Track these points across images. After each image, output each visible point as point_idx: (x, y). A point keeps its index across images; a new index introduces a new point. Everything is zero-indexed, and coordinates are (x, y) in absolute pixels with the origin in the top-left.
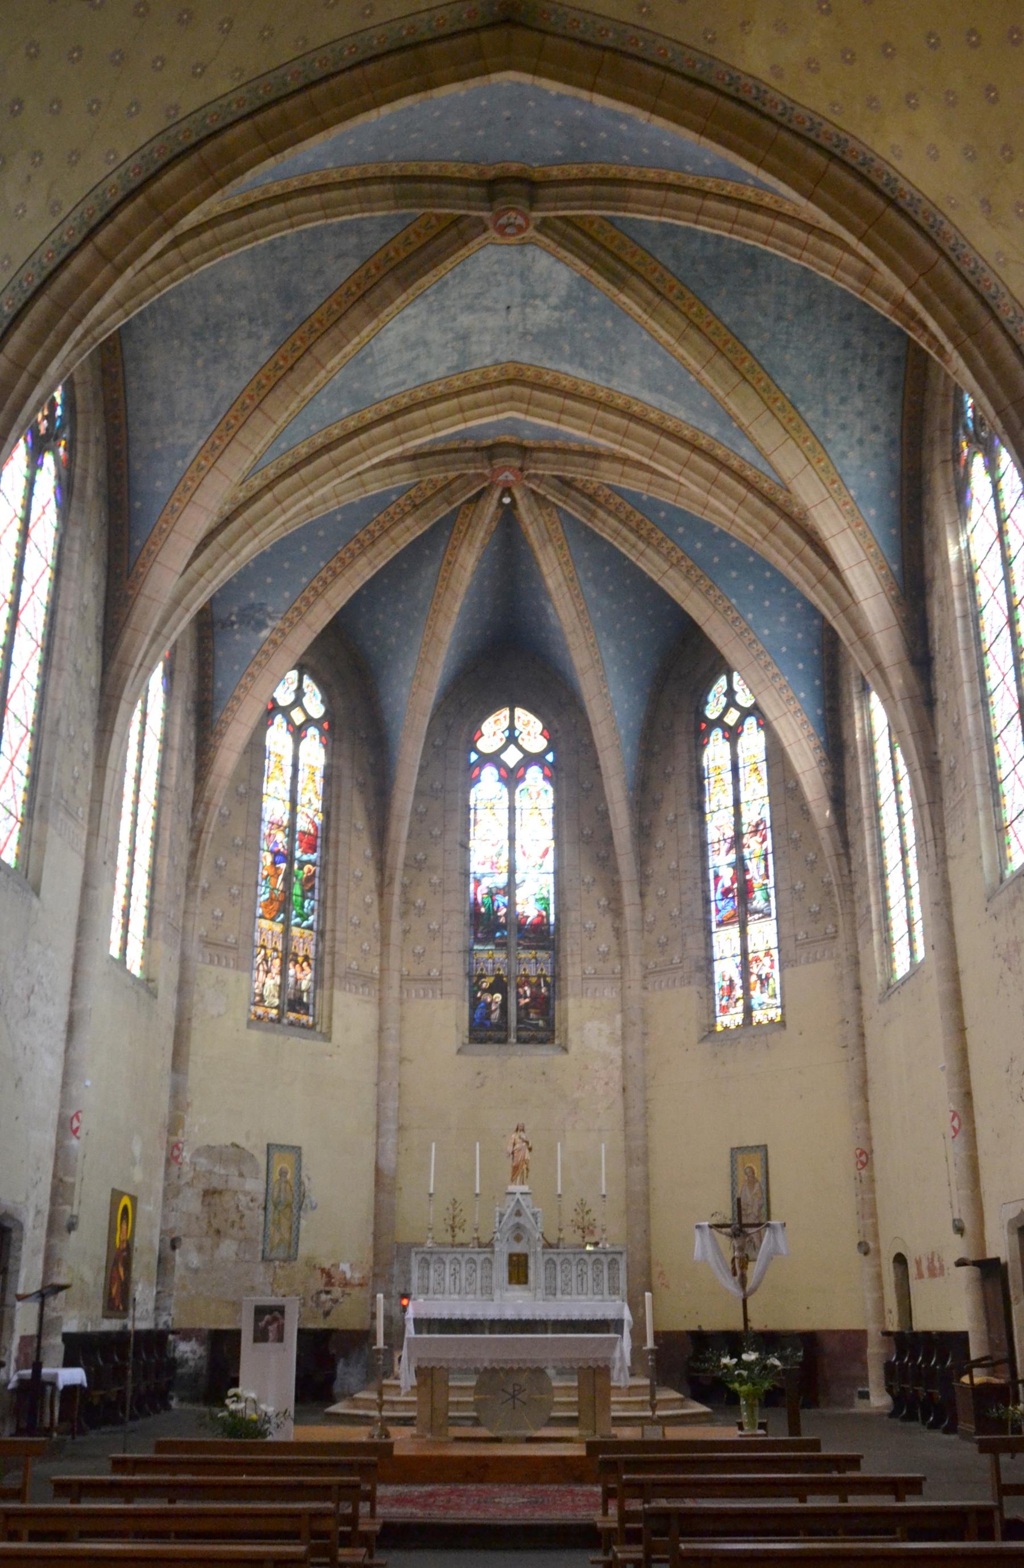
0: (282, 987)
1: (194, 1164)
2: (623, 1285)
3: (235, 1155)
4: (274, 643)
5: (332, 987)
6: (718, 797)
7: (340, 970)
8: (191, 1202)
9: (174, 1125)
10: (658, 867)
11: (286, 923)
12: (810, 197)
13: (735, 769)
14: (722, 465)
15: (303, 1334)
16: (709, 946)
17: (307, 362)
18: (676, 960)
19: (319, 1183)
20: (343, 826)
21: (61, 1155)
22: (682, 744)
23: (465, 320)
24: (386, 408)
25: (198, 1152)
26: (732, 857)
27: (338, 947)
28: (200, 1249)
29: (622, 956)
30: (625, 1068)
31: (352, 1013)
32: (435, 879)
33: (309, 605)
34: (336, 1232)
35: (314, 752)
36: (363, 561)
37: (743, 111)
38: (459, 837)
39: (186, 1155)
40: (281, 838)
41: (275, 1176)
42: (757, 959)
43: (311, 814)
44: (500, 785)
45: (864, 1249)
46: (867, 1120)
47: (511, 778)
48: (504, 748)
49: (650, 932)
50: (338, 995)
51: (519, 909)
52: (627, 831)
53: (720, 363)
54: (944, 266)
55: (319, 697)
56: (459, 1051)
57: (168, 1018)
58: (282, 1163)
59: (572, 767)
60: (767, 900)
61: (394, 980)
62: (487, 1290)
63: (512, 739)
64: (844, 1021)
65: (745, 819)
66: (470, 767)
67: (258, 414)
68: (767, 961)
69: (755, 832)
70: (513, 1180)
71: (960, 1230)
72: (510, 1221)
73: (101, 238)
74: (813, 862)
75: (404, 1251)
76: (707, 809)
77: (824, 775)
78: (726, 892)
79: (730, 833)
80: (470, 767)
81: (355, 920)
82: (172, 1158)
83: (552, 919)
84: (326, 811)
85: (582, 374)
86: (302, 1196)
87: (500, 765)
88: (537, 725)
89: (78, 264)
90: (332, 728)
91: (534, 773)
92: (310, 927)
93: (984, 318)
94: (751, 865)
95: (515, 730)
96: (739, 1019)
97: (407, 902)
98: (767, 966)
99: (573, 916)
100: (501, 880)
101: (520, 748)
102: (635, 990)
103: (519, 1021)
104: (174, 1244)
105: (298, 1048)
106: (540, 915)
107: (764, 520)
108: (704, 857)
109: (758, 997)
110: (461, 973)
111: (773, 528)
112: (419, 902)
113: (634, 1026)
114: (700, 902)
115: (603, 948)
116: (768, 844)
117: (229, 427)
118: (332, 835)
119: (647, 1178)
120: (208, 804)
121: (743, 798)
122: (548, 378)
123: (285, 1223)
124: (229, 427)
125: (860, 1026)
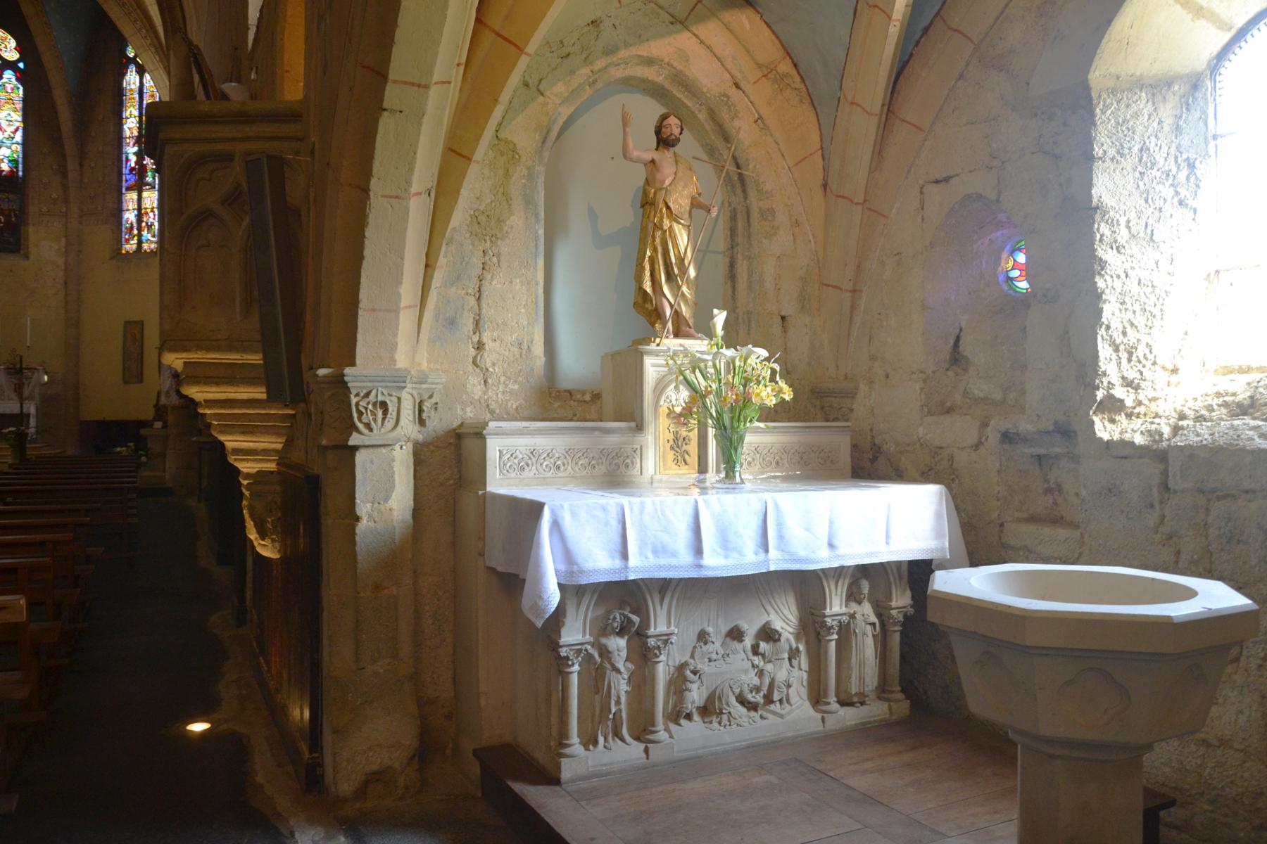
29: (66, 201)
30: (66, 270)
98: (153, 218)
106: (12, 171)
115: (54, 196)
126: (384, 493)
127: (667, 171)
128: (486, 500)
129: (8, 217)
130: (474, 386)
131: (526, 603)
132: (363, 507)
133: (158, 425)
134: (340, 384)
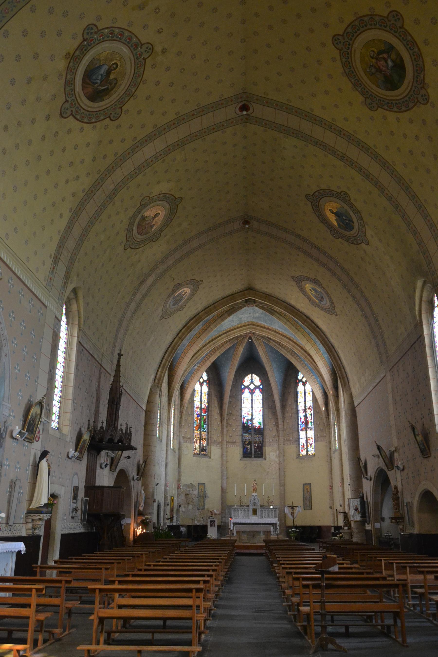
0: (200, 446)
1: (183, 488)
2: (277, 515)
3: (191, 486)
4: (198, 369)
5: (211, 445)
6: (301, 399)
7: (213, 441)
8: (183, 497)
9: (179, 480)
10: (287, 415)
12: (304, 324)
13: (305, 393)
14: (296, 343)
15: (218, 526)
16: (299, 435)
17: (209, 329)
18: (291, 438)
19: (209, 491)
20: (213, 406)
22: (293, 384)
24: (225, 332)
25: (184, 486)
26: (304, 414)
27: (212, 436)
28: (185, 507)
31: (215, 451)
32: (234, 418)
33: (206, 361)
35: (205, 388)
36: (218, 352)
37: (292, 308)
38: (240, 407)
39: (181, 486)
40: (198, 410)
41: (200, 490)
42: (309, 439)
43: (205, 404)
44: (249, 394)
45: (331, 508)
46: (332, 479)
47: (252, 392)
48: (250, 385)
49: (285, 431)
50: (212, 447)
51: (254, 425)
52: (279, 407)
53: (293, 328)
54: (326, 339)
55: (206, 375)
56: (240, 460)
57: (177, 456)
58: (201, 487)
60: (312, 425)
61: (225, 443)
62: (248, 516)
63: (252, 382)
64: (327, 456)
65: (307, 405)
66: (242, 389)
67: (199, 338)
68: (311, 440)
69: (309, 409)
70: (253, 492)
71: (341, 506)
73: (179, 335)
74: (322, 418)
76: (299, 401)
77: (323, 399)
78: (303, 422)
79: (304, 408)
80: (242, 389)
81: (216, 429)
82: (179, 488)
83: (262, 427)
84: (208, 403)
85: (265, 324)
86: (206, 495)
87: (249, 389)
88: (258, 379)
90: (209, 382)
91: (257, 391)
92: (205, 431)
93: (333, 350)
94: (308, 416)
95: (252, 380)
96: (305, 453)
98: (312, 441)
99: (267, 427)
100: (250, 418)
101: (254, 384)
102: (282, 445)
103: (254, 452)
104: (180, 506)
107: (304, 355)
108: (297, 413)
109: (310, 448)
110: (241, 440)
111: (306, 357)
112: (230, 423)
113: (282, 454)
114: (296, 425)
115: (274, 434)
116: (312, 412)
117: (193, 341)
118: (210, 409)
119: (284, 490)
120: (183, 407)
121: (306, 400)
122: (259, 324)
123: (202, 501)
124: (193, 341)
125: (331, 458)
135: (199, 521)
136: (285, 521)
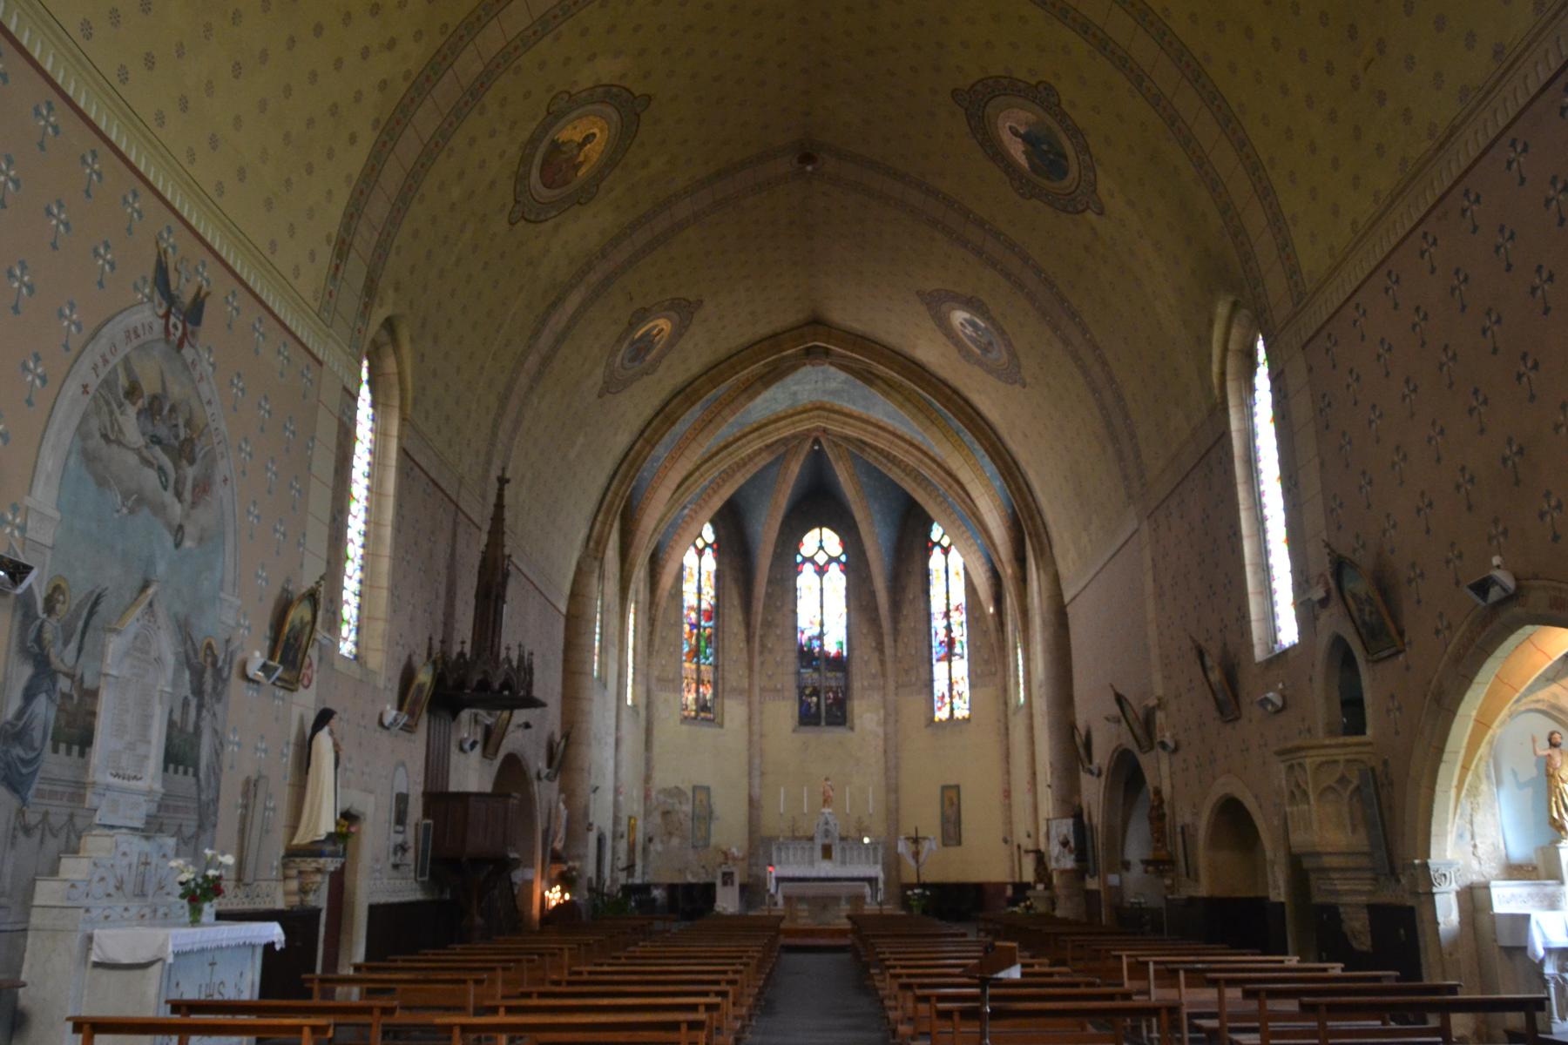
0: (697, 700)
3: (677, 792)
8: (657, 819)
9: (648, 779)
10: (903, 625)
11: (698, 663)
14: (926, 454)
16: (931, 672)
21: (616, 804)
23: (794, 388)
25: (659, 792)
26: (945, 622)
29: (884, 675)
30: (886, 740)
31: (734, 711)
34: (729, 832)
35: (709, 563)
39: (653, 794)
40: (693, 615)
45: (1005, 841)
47: (821, 571)
59: (856, 567)
61: (757, 690)
62: (812, 863)
72: (822, 828)
75: (770, 840)
82: (647, 796)
84: (717, 596)
86: (711, 813)
89: (638, 446)
90: (719, 548)
91: (834, 567)
95: (821, 542)
97: (763, 646)
98: (963, 686)
99: (857, 653)
100: (816, 631)
104: (650, 840)
105: (707, 732)
113: (891, 716)
119: (897, 801)
126: (1448, 913)
127: (1558, 759)
128: (1494, 917)
129: (836, 693)
130: (1475, 864)
131: (1529, 954)
132: (1440, 918)
133: (1040, 887)
134: (1426, 866)
135: (694, 875)
136: (898, 871)
